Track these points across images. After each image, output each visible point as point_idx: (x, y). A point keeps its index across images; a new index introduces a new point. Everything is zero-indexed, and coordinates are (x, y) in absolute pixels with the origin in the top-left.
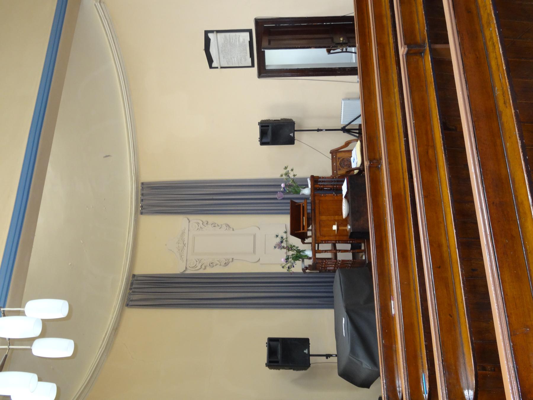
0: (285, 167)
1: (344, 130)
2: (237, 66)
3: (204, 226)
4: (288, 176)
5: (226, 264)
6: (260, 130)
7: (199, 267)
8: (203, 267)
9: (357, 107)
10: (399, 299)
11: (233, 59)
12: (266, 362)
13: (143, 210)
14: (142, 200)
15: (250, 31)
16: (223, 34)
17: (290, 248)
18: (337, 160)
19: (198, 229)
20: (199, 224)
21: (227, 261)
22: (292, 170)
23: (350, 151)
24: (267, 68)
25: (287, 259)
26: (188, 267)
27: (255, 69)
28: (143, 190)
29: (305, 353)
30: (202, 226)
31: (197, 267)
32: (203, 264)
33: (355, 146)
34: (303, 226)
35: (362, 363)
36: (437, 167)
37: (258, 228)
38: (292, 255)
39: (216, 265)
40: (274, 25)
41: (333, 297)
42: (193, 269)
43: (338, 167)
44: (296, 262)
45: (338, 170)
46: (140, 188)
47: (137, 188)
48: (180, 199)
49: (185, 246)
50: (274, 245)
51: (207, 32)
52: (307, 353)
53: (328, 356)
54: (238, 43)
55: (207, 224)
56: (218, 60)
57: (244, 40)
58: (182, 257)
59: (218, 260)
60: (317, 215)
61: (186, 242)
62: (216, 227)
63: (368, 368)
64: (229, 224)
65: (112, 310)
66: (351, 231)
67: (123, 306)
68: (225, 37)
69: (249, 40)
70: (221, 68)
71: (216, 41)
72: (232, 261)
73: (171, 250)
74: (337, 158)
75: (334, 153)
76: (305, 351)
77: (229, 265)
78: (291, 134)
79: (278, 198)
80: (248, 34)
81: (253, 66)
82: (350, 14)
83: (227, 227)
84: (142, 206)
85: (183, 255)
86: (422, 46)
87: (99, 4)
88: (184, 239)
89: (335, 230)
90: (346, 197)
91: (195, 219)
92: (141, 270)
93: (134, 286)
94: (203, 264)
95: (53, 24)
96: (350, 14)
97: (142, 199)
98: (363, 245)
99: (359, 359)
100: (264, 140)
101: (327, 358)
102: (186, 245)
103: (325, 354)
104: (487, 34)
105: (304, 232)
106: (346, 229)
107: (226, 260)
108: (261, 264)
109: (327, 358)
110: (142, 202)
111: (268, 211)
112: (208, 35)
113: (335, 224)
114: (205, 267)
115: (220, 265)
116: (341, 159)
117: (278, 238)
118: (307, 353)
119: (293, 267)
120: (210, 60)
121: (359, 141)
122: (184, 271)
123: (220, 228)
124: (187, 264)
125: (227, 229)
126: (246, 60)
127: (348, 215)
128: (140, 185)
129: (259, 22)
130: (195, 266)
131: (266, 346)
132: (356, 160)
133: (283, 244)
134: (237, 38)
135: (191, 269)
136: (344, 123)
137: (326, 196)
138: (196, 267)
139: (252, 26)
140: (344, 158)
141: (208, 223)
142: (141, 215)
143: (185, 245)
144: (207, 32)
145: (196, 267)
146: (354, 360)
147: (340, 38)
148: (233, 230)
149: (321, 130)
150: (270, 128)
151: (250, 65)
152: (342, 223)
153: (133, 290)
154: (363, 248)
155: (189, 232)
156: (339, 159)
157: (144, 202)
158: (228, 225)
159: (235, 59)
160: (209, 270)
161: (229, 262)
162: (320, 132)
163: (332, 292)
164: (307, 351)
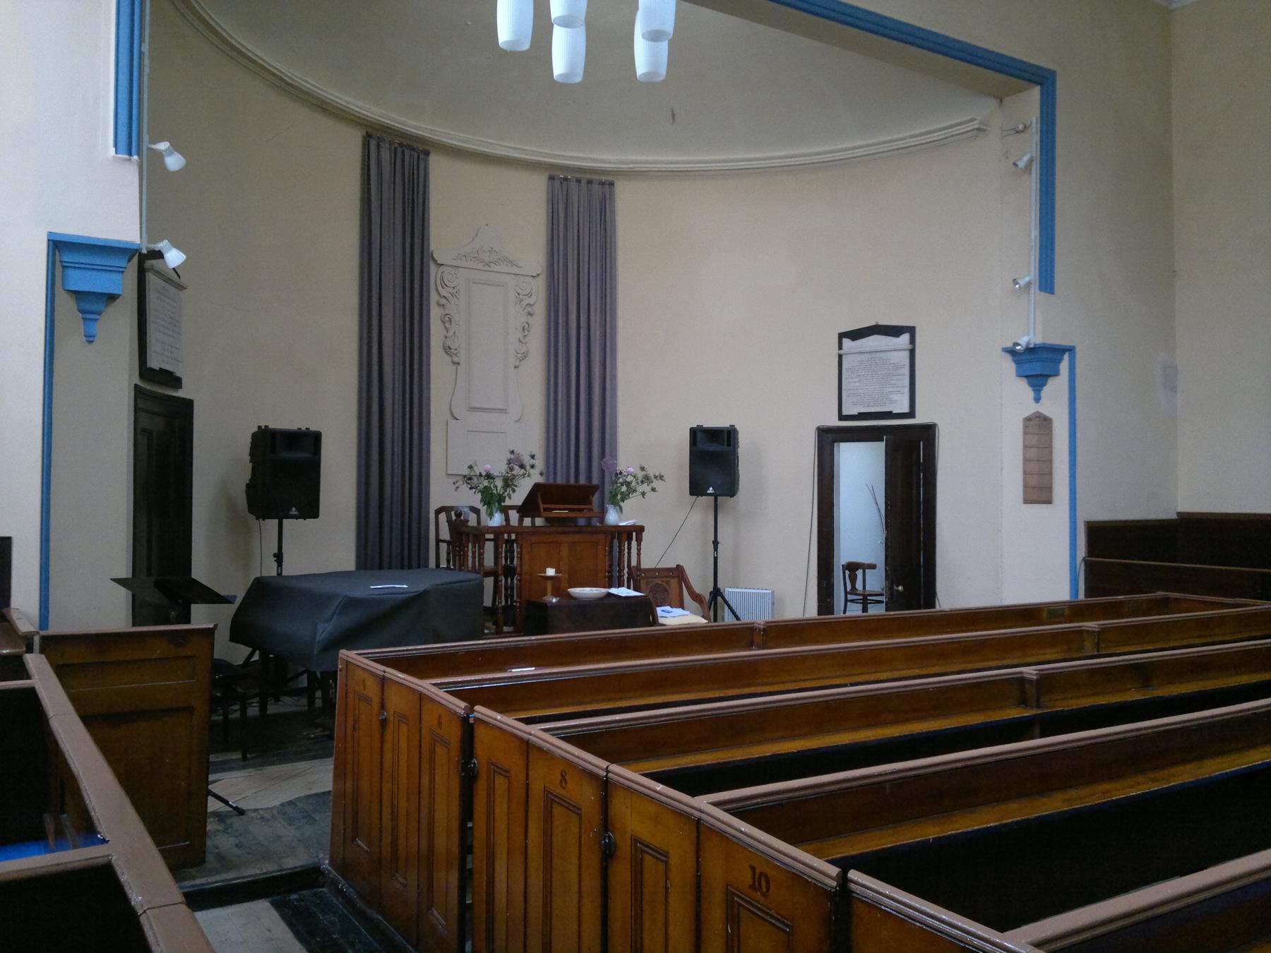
0: (663, 476)
3: (523, 306)
4: (642, 482)
5: (447, 350)
7: (443, 292)
8: (443, 301)
9: (757, 615)
10: (577, 674)
11: (857, 380)
12: (270, 427)
13: (559, 182)
14: (578, 181)
15: (911, 414)
16: (907, 362)
17: (509, 482)
18: (664, 579)
19: (518, 294)
20: (529, 297)
21: (455, 352)
22: (653, 490)
23: (682, 606)
25: (489, 476)
26: (442, 268)
27: (834, 422)
28: (599, 184)
29: (290, 510)
30: (524, 303)
32: (448, 300)
33: (693, 613)
34: (550, 510)
35: (327, 621)
36: (869, 726)
37: (520, 419)
38: (496, 487)
39: (446, 328)
40: (922, 461)
41: (381, 568)
43: (651, 580)
44: (480, 494)
45: (646, 581)
46: (604, 178)
47: (604, 172)
48: (581, 260)
49: (484, 266)
50: (517, 450)
51: (911, 330)
52: (291, 513)
53: (279, 557)
54: (891, 389)
55: (530, 314)
56: (858, 350)
57: (896, 402)
59: (457, 334)
60: (569, 538)
62: (522, 331)
63: (319, 633)
64: (527, 359)
65: (360, 103)
67: (366, 126)
69: (895, 411)
70: (840, 357)
71: (893, 348)
72: (454, 363)
74: (667, 579)
76: (294, 509)
77: (445, 355)
78: (711, 489)
79: (604, 460)
80: (906, 409)
81: (842, 417)
83: (522, 354)
84: (566, 179)
85: (466, 261)
87: (977, 126)
88: (507, 265)
89: (545, 573)
90: (609, 595)
91: (539, 289)
92: (438, 168)
93: (407, 152)
94: (448, 300)
95: (923, 30)
97: (582, 181)
99: (335, 617)
100: (699, 435)
101: (275, 555)
102: (486, 268)
103: (283, 552)
104: (1141, 779)
105: (540, 510)
106: (545, 595)
107: (456, 349)
108: (447, 421)
109: (275, 555)
110: (574, 180)
113: (556, 572)
114: (443, 305)
115: (446, 337)
116: (667, 587)
117: (529, 458)
118: (291, 513)
119: (471, 488)
120: (856, 335)
122: (435, 261)
123: (520, 341)
124: (449, 268)
125: (518, 355)
126: (855, 404)
127: (575, 598)
128: (610, 178)
129: (928, 433)
130: (444, 285)
131: (307, 429)
132: (673, 617)
133: (516, 468)
134: (899, 389)
135: (439, 276)
136: (726, 593)
137: (606, 556)
138: (444, 286)
139: (921, 418)
140: (667, 591)
141: (529, 316)
142: (547, 176)
144: (911, 330)
146: (333, 608)
148: (516, 367)
149: (716, 549)
150: (725, 448)
151: (845, 412)
153: (400, 150)
155: (513, 276)
156: (667, 582)
157: (573, 185)
158: (525, 356)
159: (857, 384)
160: (435, 313)
161: (451, 356)
163: (390, 568)
164: (295, 513)
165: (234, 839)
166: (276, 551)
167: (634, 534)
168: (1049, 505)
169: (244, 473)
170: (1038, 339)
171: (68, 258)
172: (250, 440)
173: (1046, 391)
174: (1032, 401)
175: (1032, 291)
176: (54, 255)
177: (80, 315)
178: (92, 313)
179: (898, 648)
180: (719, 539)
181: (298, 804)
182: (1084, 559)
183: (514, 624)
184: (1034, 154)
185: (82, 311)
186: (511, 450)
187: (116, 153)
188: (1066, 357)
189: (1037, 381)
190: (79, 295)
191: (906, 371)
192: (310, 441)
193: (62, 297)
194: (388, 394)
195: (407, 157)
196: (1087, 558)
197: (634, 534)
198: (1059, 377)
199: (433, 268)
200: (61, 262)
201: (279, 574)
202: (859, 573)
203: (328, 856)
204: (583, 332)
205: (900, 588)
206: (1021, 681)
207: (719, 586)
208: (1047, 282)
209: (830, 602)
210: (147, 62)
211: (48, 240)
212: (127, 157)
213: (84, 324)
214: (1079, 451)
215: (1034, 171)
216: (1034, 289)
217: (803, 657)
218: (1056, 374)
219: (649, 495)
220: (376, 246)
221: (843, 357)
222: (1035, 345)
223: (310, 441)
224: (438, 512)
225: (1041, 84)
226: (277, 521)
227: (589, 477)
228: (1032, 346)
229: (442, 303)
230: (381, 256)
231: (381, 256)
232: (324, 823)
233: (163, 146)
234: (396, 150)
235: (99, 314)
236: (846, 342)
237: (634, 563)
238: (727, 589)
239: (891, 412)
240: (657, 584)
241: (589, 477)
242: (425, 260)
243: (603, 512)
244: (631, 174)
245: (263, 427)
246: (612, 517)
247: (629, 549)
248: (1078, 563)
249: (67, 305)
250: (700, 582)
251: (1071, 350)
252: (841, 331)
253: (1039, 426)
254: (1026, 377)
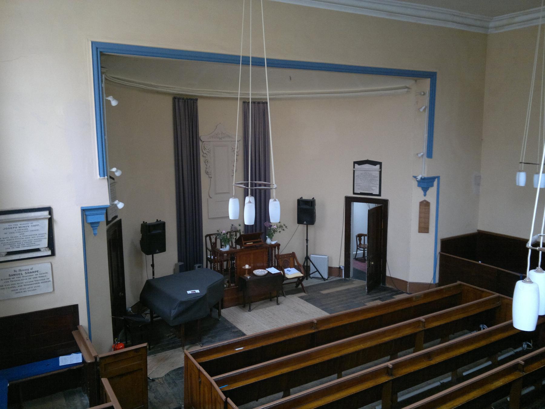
1: (307, 258)
2: (355, 182)
5: (207, 173)
6: (309, 201)
7: (204, 152)
8: (205, 155)
11: (360, 180)
15: (380, 195)
16: (378, 175)
18: (288, 258)
24: (352, 203)
27: (351, 195)
31: (205, 150)
32: (207, 154)
35: (175, 309)
42: (203, 148)
51: (380, 164)
54: (372, 185)
57: (372, 190)
58: (212, 138)
61: (223, 139)
63: (172, 314)
66: (247, 280)
68: (377, 177)
69: (374, 193)
70: (354, 171)
73: (216, 128)
75: (293, 255)
78: (305, 222)
80: (378, 193)
81: (354, 193)
82: (388, 268)
86: (392, 375)
93: (189, 101)
94: (207, 154)
96: (388, 268)
98: (234, 285)
99: (177, 308)
101: (151, 265)
102: (220, 140)
106: (245, 274)
107: (210, 172)
111: (276, 251)
112: (379, 164)
114: (205, 157)
120: (360, 163)
121: (303, 275)
122: (201, 140)
130: (205, 149)
138: (205, 149)
139: (383, 197)
142: (242, 101)
143: (220, 139)
144: (380, 164)
145: (205, 149)
147: (374, 262)
149: (307, 242)
151: (355, 192)
152: (250, 272)
153: (186, 101)
154: (232, 285)
156: (289, 259)
159: (360, 182)
160: (202, 160)
162: (306, 241)
165: (153, 394)
166: (152, 263)
167: (277, 247)
168: (428, 234)
169: (139, 236)
170: (426, 175)
171: (87, 213)
172: (140, 226)
173: (428, 192)
174: (423, 196)
175: (424, 157)
176: (83, 212)
177: (92, 228)
178: (95, 227)
179: (357, 339)
180: (308, 239)
181: (170, 375)
182: (439, 253)
183: (234, 283)
184: (427, 105)
185: (92, 227)
186: (232, 224)
187: (100, 177)
188: (436, 180)
189: (425, 190)
190: (92, 224)
191: (378, 179)
192: (161, 226)
193: (86, 224)
194: (187, 199)
195: (189, 103)
196: (440, 253)
197: (277, 247)
198: (433, 187)
199: (201, 143)
200: (85, 214)
201: (154, 278)
202: (363, 238)
203: (183, 403)
204: (257, 161)
205: (372, 263)
206: (387, 368)
207: (308, 255)
208: (430, 154)
209: (349, 260)
210: (107, 142)
211: (81, 210)
212: (103, 178)
213: (93, 230)
214: (439, 216)
215: (426, 111)
216: (425, 156)
217: (325, 349)
218: (432, 186)
219: (282, 232)
220: (180, 144)
221: (355, 171)
222: (424, 177)
223: (161, 226)
224: (206, 236)
225: (431, 78)
226: (151, 255)
227: (261, 230)
228: (423, 178)
229: (204, 156)
230: (181, 146)
231: (181, 146)
232: (181, 385)
233: (114, 169)
234: (185, 101)
235: (97, 227)
236: (356, 165)
237: (277, 253)
238: (311, 255)
239: (372, 193)
240: (286, 260)
241: (261, 230)
242: (198, 140)
243: (266, 239)
244: (202, 97)
245: (145, 222)
246: (269, 241)
247: (275, 251)
248: (437, 254)
249: (88, 227)
250: (300, 258)
251: (438, 177)
252: (354, 161)
253: (425, 205)
254: (422, 187)
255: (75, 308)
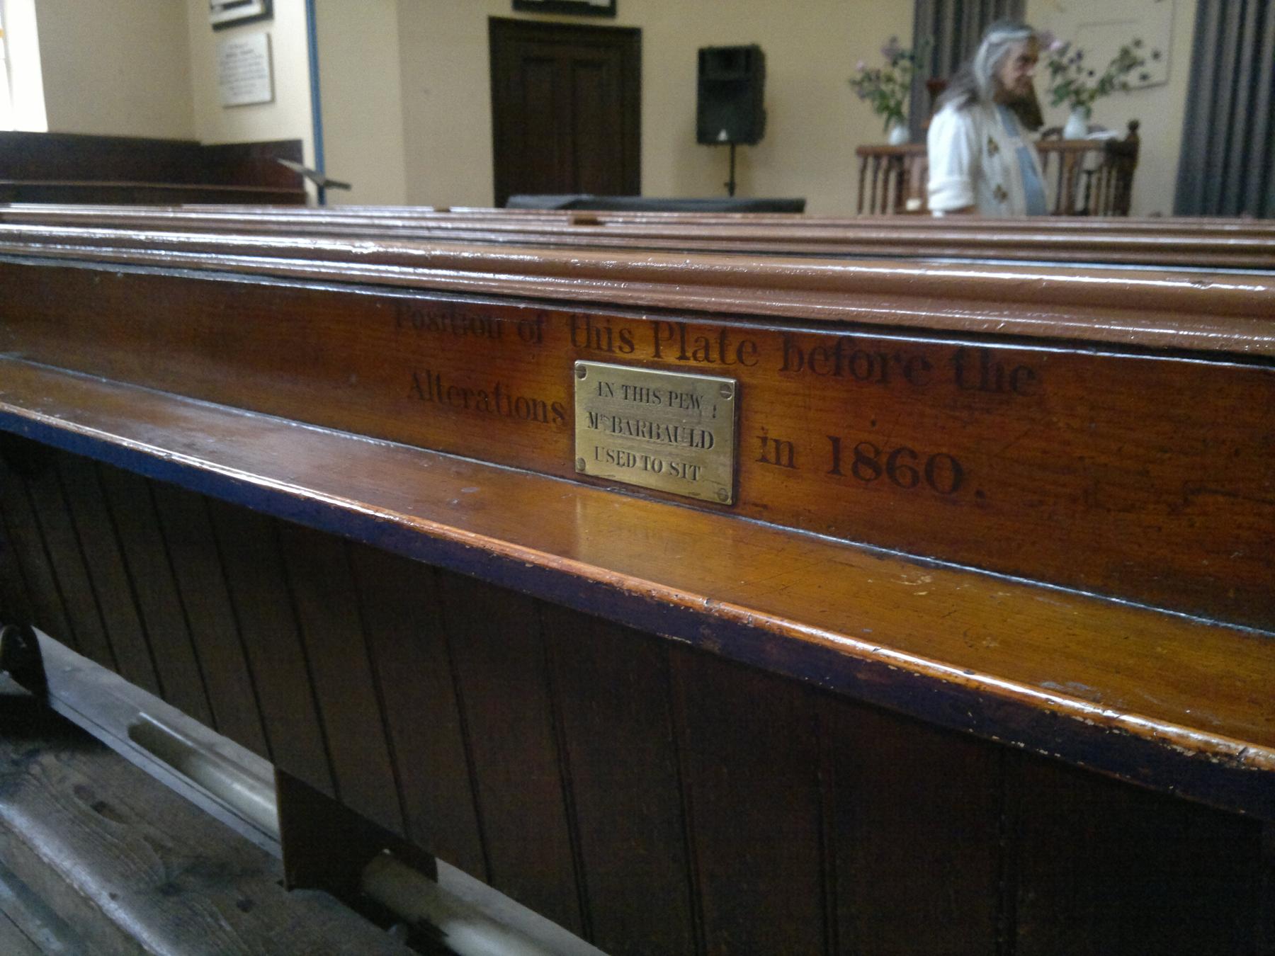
15: (610, 11)
255: (292, 149)
